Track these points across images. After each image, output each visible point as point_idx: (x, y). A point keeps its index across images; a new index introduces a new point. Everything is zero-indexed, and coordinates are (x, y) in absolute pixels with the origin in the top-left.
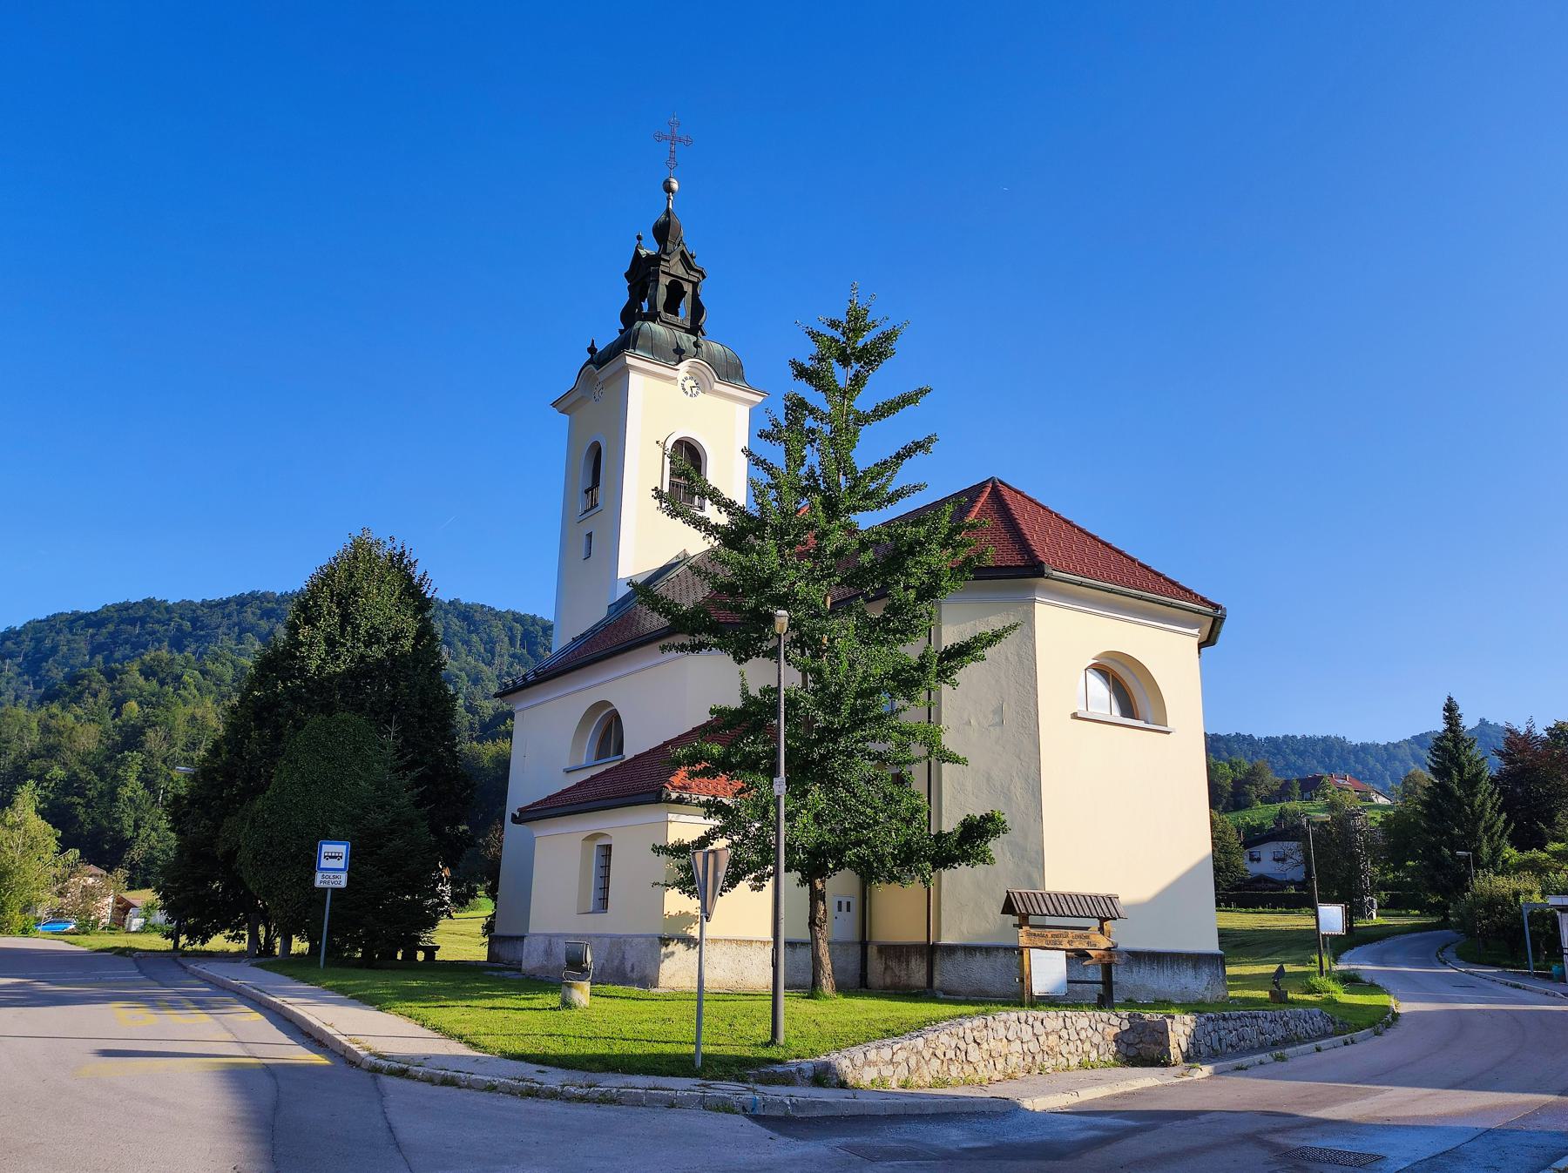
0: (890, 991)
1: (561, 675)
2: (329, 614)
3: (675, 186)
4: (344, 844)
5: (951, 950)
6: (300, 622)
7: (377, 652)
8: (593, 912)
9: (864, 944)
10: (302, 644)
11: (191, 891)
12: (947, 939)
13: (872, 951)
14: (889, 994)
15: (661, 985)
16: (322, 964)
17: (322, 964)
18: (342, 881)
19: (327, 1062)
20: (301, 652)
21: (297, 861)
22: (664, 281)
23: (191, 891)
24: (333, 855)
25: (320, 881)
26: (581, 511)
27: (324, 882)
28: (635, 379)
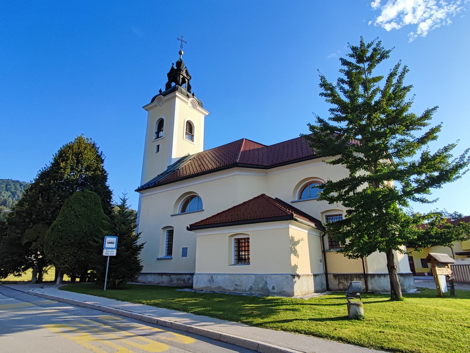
0: (342, 292)
1: (169, 183)
2: (72, 159)
3: (183, 53)
4: (106, 238)
5: (373, 276)
6: (60, 161)
7: (90, 174)
8: (234, 265)
9: (326, 274)
10: (61, 168)
11: (10, 258)
12: (370, 272)
13: (331, 277)
14: (342, 292)
15: (295, 295)
16: (105, 289)
17: (105, 289)
18: (114, 253)
19: (76, 329)
20: (61, 171)
21: (73, 245)
22: (181, 77)
23: (10, 258)
24: (111, 242)
25: (105, 253)
26: (154, 139)
27: (107, 254)
28: (177, 100)
